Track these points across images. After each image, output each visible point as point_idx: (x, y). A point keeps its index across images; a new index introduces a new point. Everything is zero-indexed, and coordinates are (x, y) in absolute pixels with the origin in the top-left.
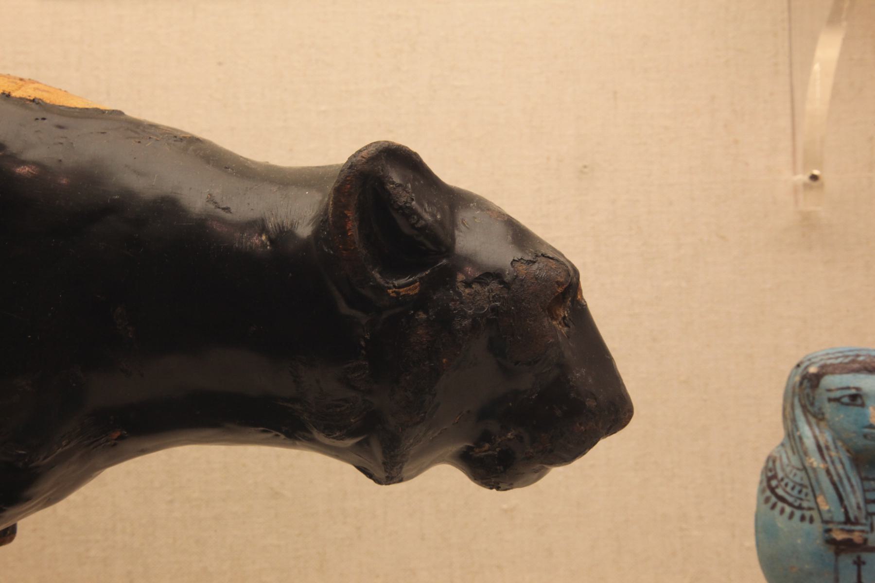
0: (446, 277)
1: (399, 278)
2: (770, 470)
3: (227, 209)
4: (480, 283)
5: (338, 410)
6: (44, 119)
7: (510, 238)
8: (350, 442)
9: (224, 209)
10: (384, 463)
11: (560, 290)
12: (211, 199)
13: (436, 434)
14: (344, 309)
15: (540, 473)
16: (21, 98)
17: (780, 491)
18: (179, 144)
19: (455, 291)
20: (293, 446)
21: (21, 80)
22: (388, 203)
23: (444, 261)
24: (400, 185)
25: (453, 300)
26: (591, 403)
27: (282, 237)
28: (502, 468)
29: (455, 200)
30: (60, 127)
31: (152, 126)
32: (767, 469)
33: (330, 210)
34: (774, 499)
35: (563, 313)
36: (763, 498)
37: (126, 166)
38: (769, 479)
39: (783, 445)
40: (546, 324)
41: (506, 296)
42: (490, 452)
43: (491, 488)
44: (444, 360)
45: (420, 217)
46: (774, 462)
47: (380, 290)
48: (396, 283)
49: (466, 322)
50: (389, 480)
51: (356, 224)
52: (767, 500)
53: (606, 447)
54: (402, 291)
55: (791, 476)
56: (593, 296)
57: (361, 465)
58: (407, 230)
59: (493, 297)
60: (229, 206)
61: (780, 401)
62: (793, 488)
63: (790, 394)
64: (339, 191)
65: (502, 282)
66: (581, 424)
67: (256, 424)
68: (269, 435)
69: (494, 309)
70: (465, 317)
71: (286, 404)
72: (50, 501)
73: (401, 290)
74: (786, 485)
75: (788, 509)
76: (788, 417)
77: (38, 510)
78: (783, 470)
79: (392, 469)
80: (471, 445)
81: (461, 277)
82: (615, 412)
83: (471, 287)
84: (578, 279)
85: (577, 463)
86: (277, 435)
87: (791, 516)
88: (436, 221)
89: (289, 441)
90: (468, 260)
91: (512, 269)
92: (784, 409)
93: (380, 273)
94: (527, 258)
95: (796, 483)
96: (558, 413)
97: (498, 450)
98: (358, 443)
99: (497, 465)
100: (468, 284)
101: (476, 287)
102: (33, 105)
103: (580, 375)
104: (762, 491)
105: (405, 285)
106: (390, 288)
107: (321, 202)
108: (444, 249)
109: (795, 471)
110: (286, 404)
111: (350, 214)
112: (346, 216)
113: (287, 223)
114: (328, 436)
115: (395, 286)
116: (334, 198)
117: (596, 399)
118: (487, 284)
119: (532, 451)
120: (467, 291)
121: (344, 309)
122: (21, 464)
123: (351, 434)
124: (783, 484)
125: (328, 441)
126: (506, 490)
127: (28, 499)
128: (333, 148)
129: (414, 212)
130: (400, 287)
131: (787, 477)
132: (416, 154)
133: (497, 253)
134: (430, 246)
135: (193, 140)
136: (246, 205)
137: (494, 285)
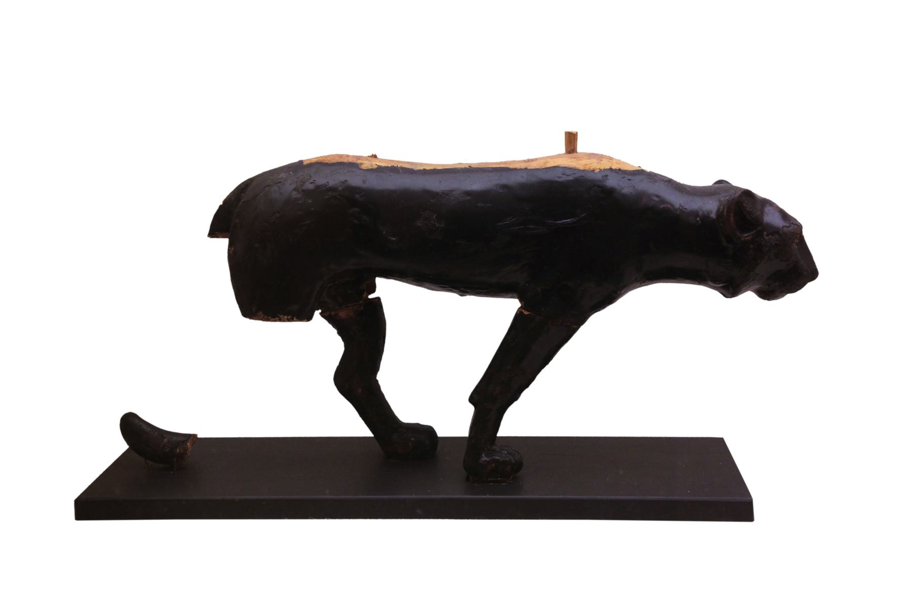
26: (805, 273)
27: (705, 218)
99: (768, 293)
105: (747, 236)
133: (778, 222)
136: (694, 204)
137: (777, 236)
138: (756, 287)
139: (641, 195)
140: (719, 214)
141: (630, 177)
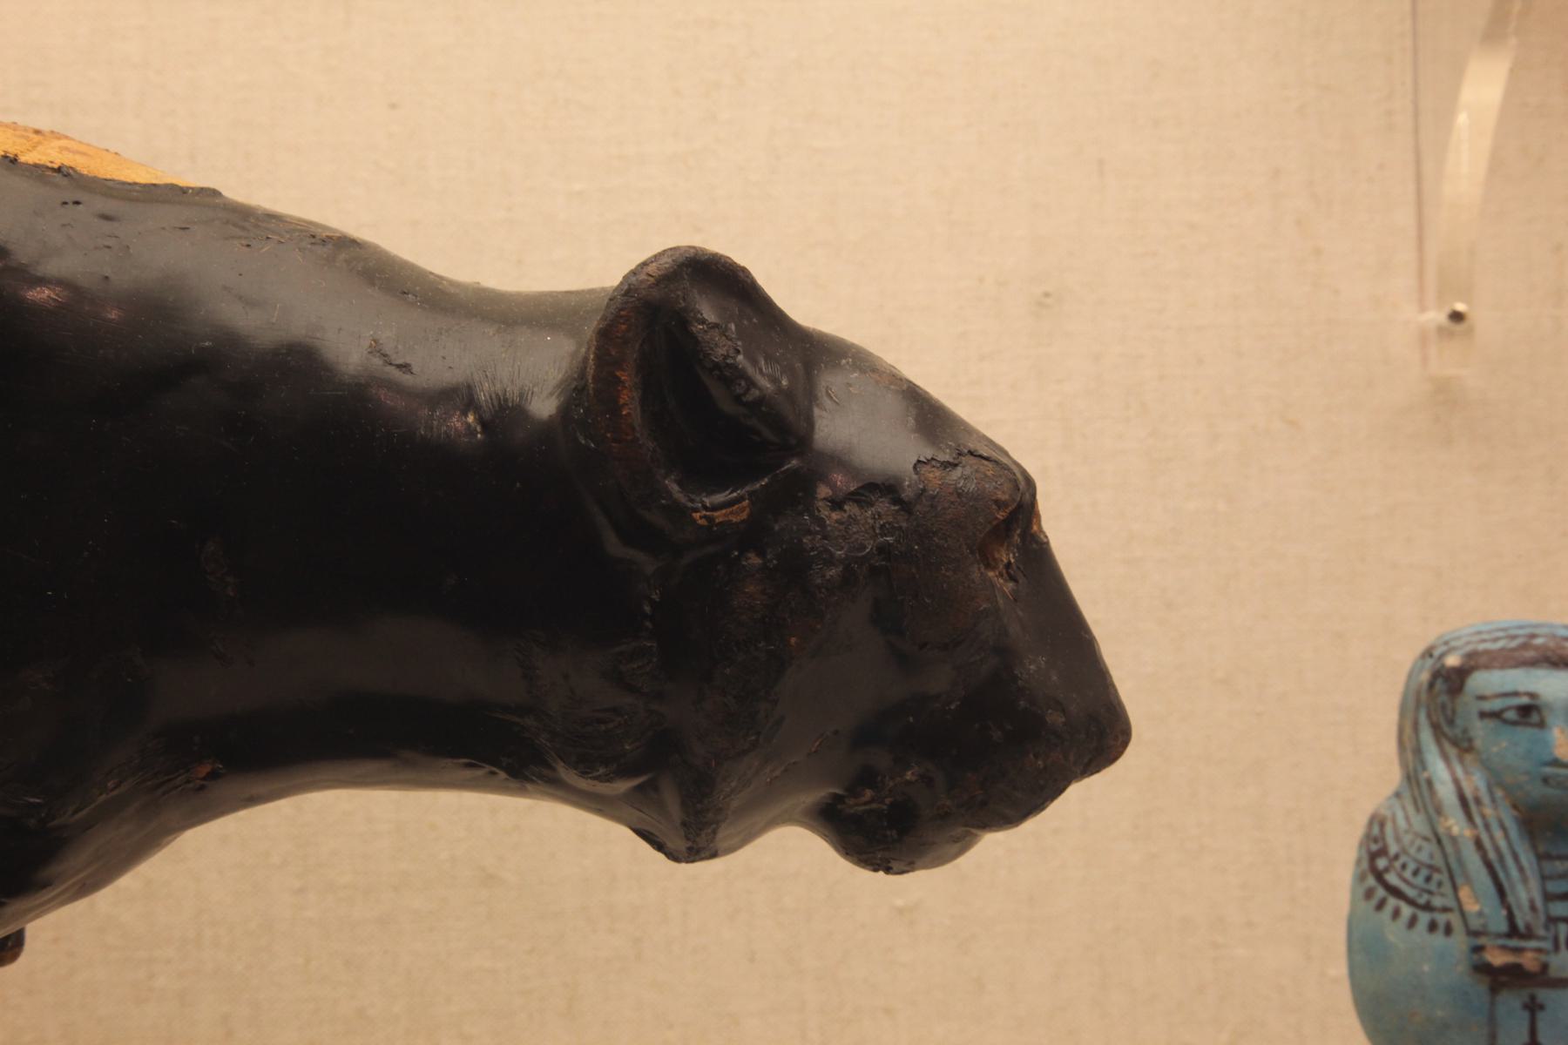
1: (709, 494)
2: (1376, 841)
3: (405, 367)
4: (856, 501)
5: (603, 727)
6: (77, 203)
7: (911, 421)
8: (623, 786)
9: (399, 366)
10: (684, 824)
11: (1001, 515)
12: (376, 349)
13: (777, 773)
14: (613, 545)
15: (963, 844)
16: (36, 166)
17: (1392, 879)
18: (320, 250)
19: (812, 515)
20: (522, 792)
21: (37, 132)
22: (693, 358)
25: (809, 532)
26: (1055, 718)
27: (504, 417)
29: (815, 352)
30: (107, 218)
31: (272, 217)
32: (1369, 838)
33: (591, 371)
34: (1381, 892)
35: (1006, 556)
36: (1361, 891)
37: (225, 288)
38: (1373, 857)
39: (1398, 795)
40: (976, 575)
41: (904, 525)
42: (874, 806)
43: (876, 870)
44: (793, 640)
45: (751, 383)
46: (1382, 825)
47: (679, 513)
50: (694, 853)
51: (636, 395)
52: (1369, 894)
54: (719, 516)
55: (1412, 851)
57: (638, 826)
58: (727, 406)
59: (882, 527)
62: (1415, 873)
63: (1411, 705)
66: (1036, 756)
67: (453, 754)
68: (479, 773)
69: (882, 550)
70: (830, 561)
72: (86, 888)
74: (1404, 866)
75: (1407, 911)
78: (1398, 839)
81: (823, 491)
82: (1098, 734)
84: (1034, 495)
85: (1030, 825)
86: (493, 773)
87: (1412, 922)
88: (780, 390)
89: (513, 784)
90: (838, 461)
93: (680, 483)
97: (888, 801)
98: (640, 788)
99: (883, 832)
100: (836, 504)
102: (58, 177)
103: (1035, 667)
104: (1361, 878)
105: (723, 506)
106: (696, 510)
108: (793, 441)
109: (1419, 842)
111: (626, 376)
112: (618, 381)
113: (512, 392)
114: (583, 774)
115: (705, 508)
116: (598, 348)
118: (872, 505)
119: (948, 803)
120: (835, 516)
122: (32, 822)
123: (625, 772)
124: (1397, 864)
125: (583, 784)
127: (45, 885)
128: (587, 252)
129: (742, 375)
130: (714, 508)
131: (1405, 851)
132: (744, 270)
133: (889, 448)
134: (768, 434)
136: (441, 358)
137: (883, 506)
138: (812, 797)
139: (157, 309)
140: (576, 394)
141: (110, 206)
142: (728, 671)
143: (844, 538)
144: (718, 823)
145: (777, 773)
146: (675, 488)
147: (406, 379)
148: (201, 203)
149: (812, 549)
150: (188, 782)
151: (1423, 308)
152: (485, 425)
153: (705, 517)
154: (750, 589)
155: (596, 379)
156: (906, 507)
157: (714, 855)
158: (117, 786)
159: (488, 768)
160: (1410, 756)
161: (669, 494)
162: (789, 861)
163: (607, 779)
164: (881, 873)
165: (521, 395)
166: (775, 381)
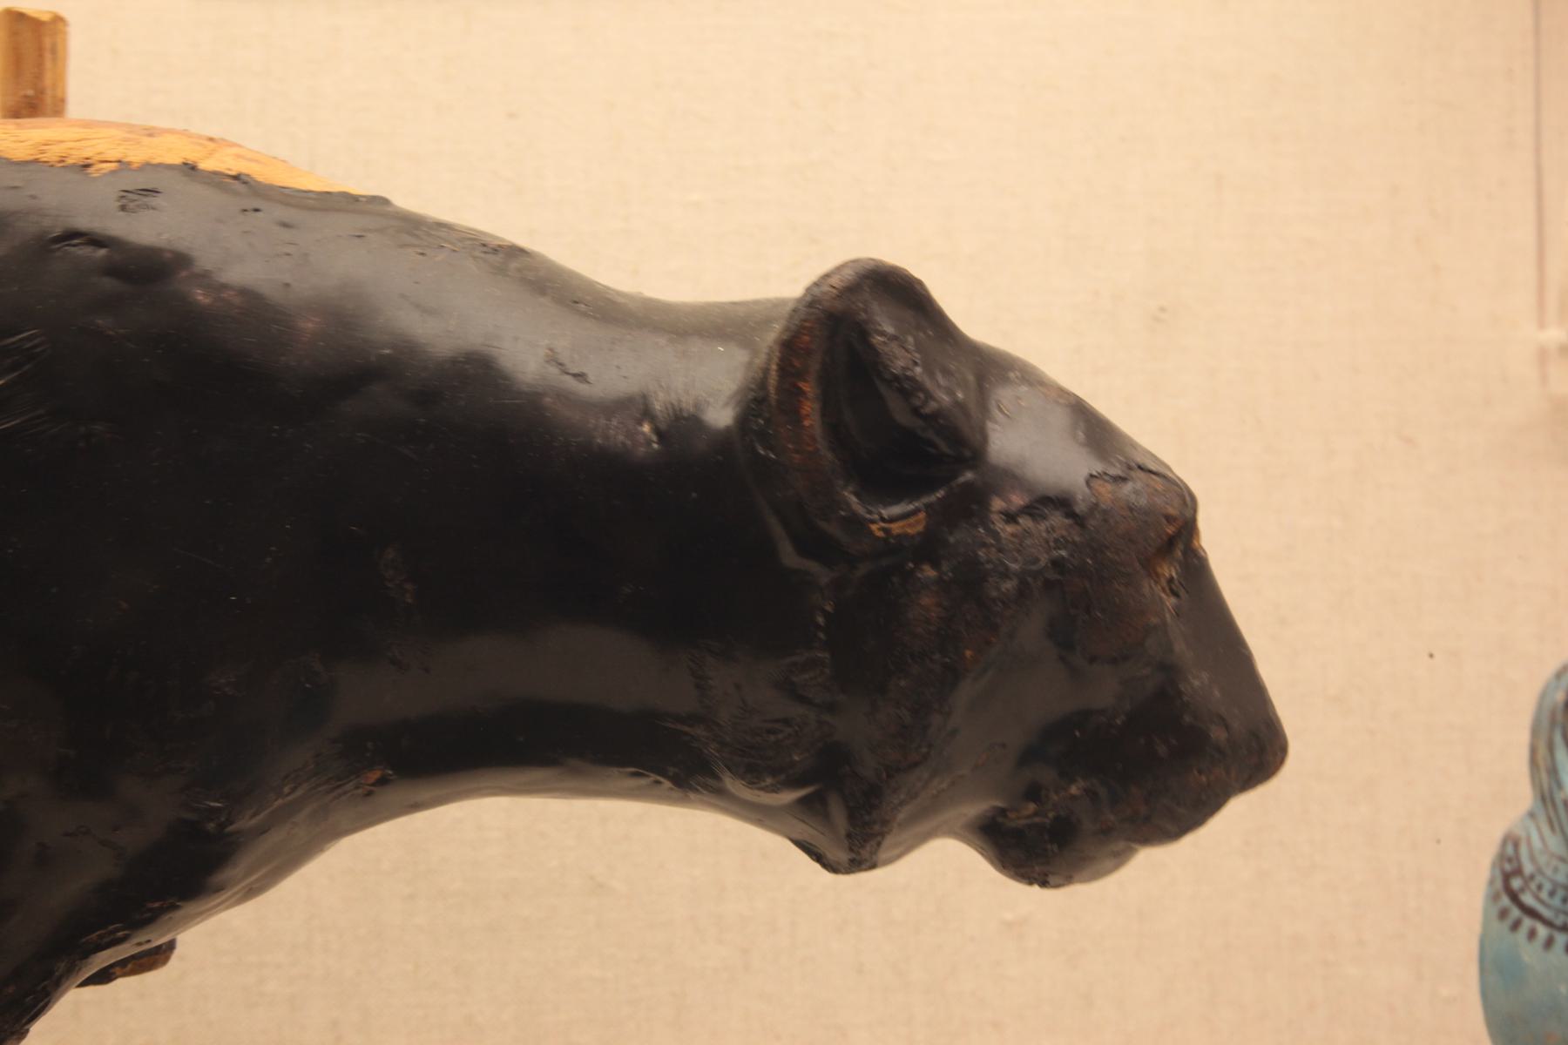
0: (970, 506)
1: (886, 505)
2: (1510, 860)
3: (580, 377)
4: (1031, 515)
5: (772, 738)
6: (257, 210)
7: (1081, 436)
8: (788, 797)
9: (575, 375)
10: (849, 836)
11: (1170, 530)
12: (553, 359)
13: (944, 786)
14: (789, 557)
15: (1121, 858)
16: (215, 173)
17: (1528, 899)
18: (491, 258)
19: (987, 529)
20: (683, 801)
21: (211, 139)
22: (867, 370)
23: (969, 476)
24: (894, 338)
25: (984, 545)
26: (1218, 734)
27: (681, 428)
28: (1055, 847)
29: (990, 368)
30: (285, 225)
31: (441, 225)
32: (1502, 857)
33: (773, 380)
34: (1516, 912)
35: (1168, 570)
36: (1494, 912)
37: (403, 296)
38: (1507, 877)
39: (1532, 815)
40: (1146, 590)
41: (1077, 539)
42: (1037, 820)
43: (1031, 883)
44: (968, 653)
45: (929, 396)
46: (1516, 845)
47: (857, 524)
48: (885, 513)
49: (1009, 586)
50: (857, 864)
51: (816, 406)
52: (1503, 914)
53: (1240, 811)
54: (896, 528)
55: (1549, 872)
56: (1221, 542)
57: (795, 836)
58: (902, 416)
59: (1056, 541)
60: (585, 370)
61: (1523, 738)
62: (1552, 894)
63: (1545, 723)
64: (791, 348)
65: (1071, 514)
66: (1200, 772)
67: (621, 763)
68: (643, 782)
69: (1057, 564)
70: (1006, 574)
71: (679, 727)
72: (252, 892)
73: (893, 526)
74: (1540, 887)
75: (1543, 931)
76: (1541, 763)
77: (228, 908)
78: (1533, 859)
79: (862, 847)
80: (999, 804)
81: (997, 504)
82: (1256, 750)
83: (1017, 523)
84: (1195, 510)
85: (1188, 840)
86: (658, 782)
87: (1549, 943)
88: (957, 404)
89: (677, 793)
90: (1008, 477)
91: (1087, 490)
92: (1533, 751)
93: (857, 495)
94: (1113, 471)
95: (1555, 885)
96: (1162, 750)
97: (1051, 815)
98: (802, 801)
99: (1036, 847)
100: (1010, 518)
101: (1025, 522)
102: (236, 185)
103: (1199, 682)
104: (1495, 897)
105: (899, 517)
106: (873, 522)
107: (750, 364)
108: (968, 454)
109: (1555, 862)
110: (679, 727)
111: (809, 387)
112: (802, 393)
113: (687, 404)
114: (751, 784)
115: (883, 520)
116: (782, 359)
117: (1227, 727)
118: (1044, 518)
119: (1112, 817)
120: (1010, 529)
121: (789, 557)
122: (211, 826)
123: (793, 783)
124: (1533, 886)
125: (748, 794)
126: (1057, 886)
127: (219, 889)
128: (775, 266)
129: (918, 387)
130: (892, 520)
131: (1540, 871)
132: (920, 283)
133: (1062, 464)
134: (944, 447)
135: (515, 252)
136: (614, 372)
137: (1057, 519)
138: (975, 809)
142: (903, 683)
143: (1019, 551)
144: (883, 835)
145: (944, 786)
146: (853, 499)
147: (582, 389)
148: (367, 211)
149: (989, 561)
150: (357, 788)
151: (1542, 325)
152: (657, 431)
153: (883, 529)
154: (926, 600)
155: (779, 389)
156: (1079, 520)
157: (873, 866)
158: (293, 790)
159: (654, 777)
160: (1544, 776)
161: (848, 504)
162: (942, 873)
163: (774, 789)
164: (1036, 888)
165: (697, 406)
166: (951, 392)
